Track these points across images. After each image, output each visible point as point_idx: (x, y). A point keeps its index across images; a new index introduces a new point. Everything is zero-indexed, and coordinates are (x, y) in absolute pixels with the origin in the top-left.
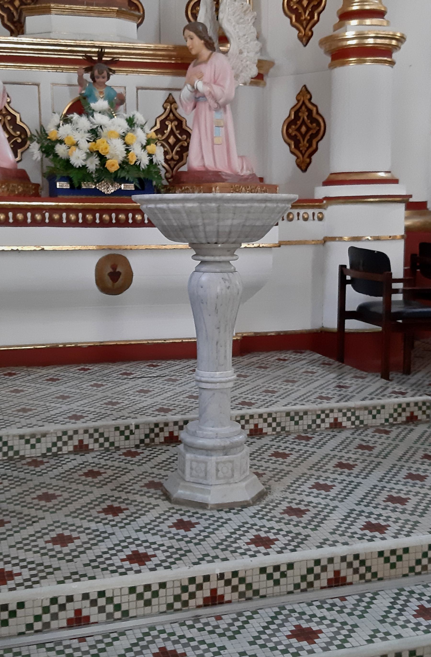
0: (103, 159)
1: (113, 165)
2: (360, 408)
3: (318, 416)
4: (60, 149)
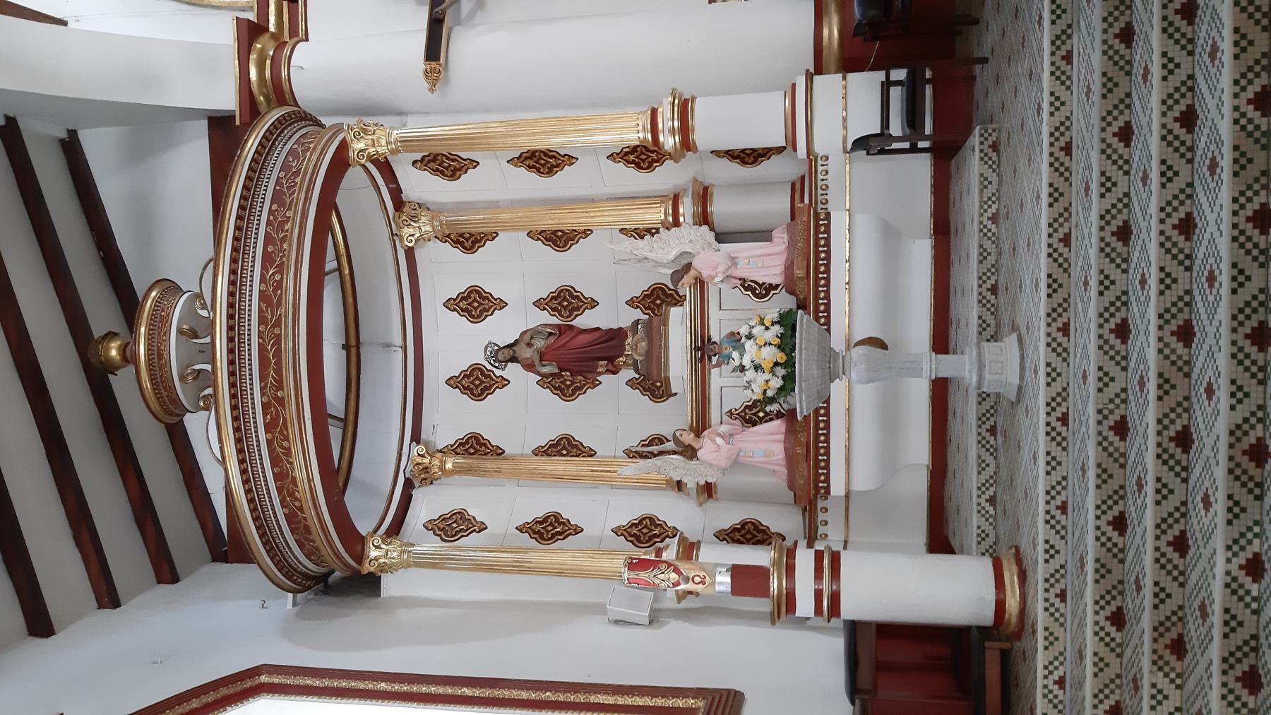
0: (776, 364)
1: (781, 357)
2: (981, 197)
3: (985, 235)
4: (770, 393)
